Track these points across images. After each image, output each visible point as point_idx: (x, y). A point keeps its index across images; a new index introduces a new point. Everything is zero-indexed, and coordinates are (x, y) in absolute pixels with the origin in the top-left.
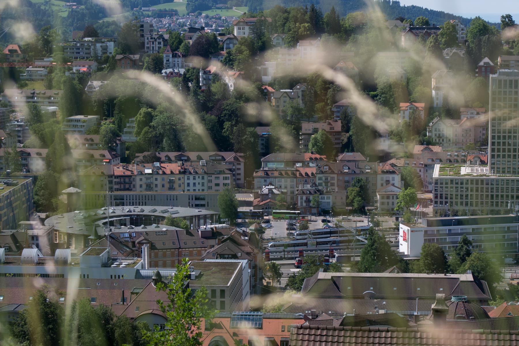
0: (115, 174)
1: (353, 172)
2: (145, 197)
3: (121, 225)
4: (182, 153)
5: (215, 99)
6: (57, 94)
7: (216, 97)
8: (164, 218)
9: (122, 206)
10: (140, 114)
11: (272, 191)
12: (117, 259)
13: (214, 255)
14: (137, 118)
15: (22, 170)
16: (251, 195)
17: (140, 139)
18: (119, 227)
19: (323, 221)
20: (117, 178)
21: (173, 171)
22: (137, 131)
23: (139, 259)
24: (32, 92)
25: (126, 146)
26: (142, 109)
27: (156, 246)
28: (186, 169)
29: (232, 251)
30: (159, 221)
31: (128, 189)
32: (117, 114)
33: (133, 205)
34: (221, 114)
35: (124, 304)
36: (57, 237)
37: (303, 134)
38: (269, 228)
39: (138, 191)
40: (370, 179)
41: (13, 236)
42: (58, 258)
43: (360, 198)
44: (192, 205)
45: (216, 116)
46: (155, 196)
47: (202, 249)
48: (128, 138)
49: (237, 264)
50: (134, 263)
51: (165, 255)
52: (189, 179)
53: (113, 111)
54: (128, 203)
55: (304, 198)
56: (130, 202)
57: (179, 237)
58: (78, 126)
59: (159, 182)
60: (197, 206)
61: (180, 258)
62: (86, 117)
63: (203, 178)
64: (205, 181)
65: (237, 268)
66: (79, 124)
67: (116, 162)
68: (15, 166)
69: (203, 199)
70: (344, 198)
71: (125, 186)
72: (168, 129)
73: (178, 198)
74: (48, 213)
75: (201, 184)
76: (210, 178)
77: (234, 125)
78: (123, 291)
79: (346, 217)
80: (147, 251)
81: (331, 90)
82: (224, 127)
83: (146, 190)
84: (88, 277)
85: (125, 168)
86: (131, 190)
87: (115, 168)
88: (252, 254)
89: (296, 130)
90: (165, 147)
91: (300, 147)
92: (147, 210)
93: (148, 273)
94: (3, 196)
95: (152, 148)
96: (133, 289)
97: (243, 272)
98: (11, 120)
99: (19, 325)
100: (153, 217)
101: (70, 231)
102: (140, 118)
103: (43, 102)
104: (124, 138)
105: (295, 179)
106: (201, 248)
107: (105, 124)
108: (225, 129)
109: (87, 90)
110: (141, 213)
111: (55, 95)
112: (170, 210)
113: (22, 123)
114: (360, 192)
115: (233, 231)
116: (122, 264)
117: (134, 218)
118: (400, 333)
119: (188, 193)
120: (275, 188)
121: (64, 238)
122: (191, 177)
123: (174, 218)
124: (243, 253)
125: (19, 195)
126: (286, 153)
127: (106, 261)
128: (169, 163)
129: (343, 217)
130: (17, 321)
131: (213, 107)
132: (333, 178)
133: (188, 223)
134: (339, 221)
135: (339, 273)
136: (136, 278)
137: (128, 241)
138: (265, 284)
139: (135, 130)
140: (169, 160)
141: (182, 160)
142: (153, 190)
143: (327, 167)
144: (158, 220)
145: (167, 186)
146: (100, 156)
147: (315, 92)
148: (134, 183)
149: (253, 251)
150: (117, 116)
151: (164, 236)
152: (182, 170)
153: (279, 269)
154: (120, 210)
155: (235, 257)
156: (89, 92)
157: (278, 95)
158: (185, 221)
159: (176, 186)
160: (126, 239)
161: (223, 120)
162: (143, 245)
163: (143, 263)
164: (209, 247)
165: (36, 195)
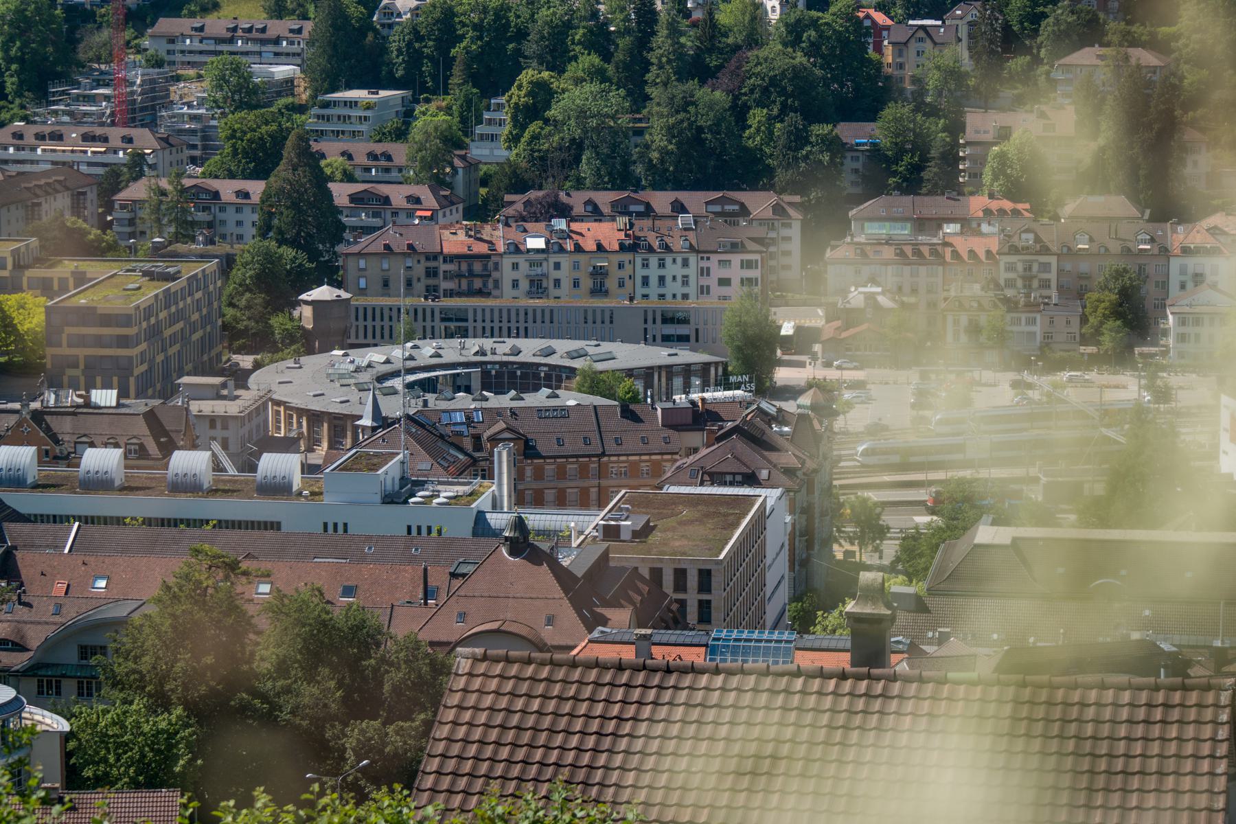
0: (446, 251)
1: (1102, 250)
2: (526, 314)
3: (458, 389)
4: (632, 195)
5: (728, 45)
6: (299, 31)
7: (730, 40)
8: (572, 371)
9: (462, 337)
10: (520, 87)
11: (876, 300)
12: (426, 482)
13: (693, 475)
14: (511, 97)
15: (194, 237)
16: (820, 312)
17: (517, 154)
18: (448, 393)
19: (1015, 385)
20: (451, 261)
21: (602, 242)
22: (511, 133)
23: (486, 482)
24: (231, 26)
25: (482, 173)
26: (524, 72)
27: (538, 448)
28: (638, 238)
29: (744, 464)
30: (559, 380)
31: (481, 293)
32: (459, 85)
33: (492, 336)
34: (740, 88)
35: (426, 604)
36: (280, 422)
37: (968, 144)
38: (863, 403)
39: (509, 298)
40: (1150, 270)
41: (151, 417)
42: (275, 477)
43: (1118, 323)
44: (654, 336)
45: (729, 92)
46: (552, 311)
47: (666, 457)
48: (486, 152)
49: (748, 501)
50: (471, 494)
51: (561, 474)
52: (647, 265)
53: (447, 78)
54: (480, 331)
55: (964, 320)
56: (484, 328)
57: (602, 424)
58: (353, 120)
59: (565, 274)
60: (667, 339)
61: (604, 483)
62: (373, 93)
63: (685, 263)
64: (692, 271)
65: (750, 511)
66: (355, 113)
67: (450, 218)
68: (177, 228)
69: (685, 321)
70: (1076, 321)
71: (470, 284)
72: (593, 129)
73: (614, 316)
74: (259, 357)
75: (679, 279)
76: (704, 264)
77: (777, 117)
78: (425, 570)
79: (1078, 373)
80: (508, 461)
81: (1051, 20)
82: (749, 122)
83: (530, 294)
84: (346, 531)
85: (472, 233)
86: (488, 295)
87: (446, 233)
88: (799, 474)
89: (949, 132)
90: (585, 178)
91: (961, 180)
92: (529, 349)
93: (536, 523)
94: (137, 308)
95: (551, 179)
96: (456, 563)
97: (769, 523)
98: (172, 101)
99: (128, 655)
100: (545, 369)
101: (316, 406)
102: (519, 96)
103: (260, 53)
104: (478, 151)
105: (940, 268)
106: (640, 455)
107: (424, 114)
108: (752, 130)
109: (378, 19)
110: (512, 359)
111: (291, 35)
112: (591, 350)
113: (200, 111)
114: (1121, 305)
115: (749, 410)
116: (438, 496)
117: (493, 372)
118: (748, 677)
119: (644, 304)
120: (883, 293)
121: (300, 425)
122: (653, 261)
123: (601, 372)
124: (774, 472)
125: (181, 305)
126: (920, 194)
127: (397, 487)
128: (596, 221)
129: (1073, 373)
130: (124, 644)
131: (720, 68)
132: (1045, 267)
133: (639, 386)
134: (1056, 386)
135: (1102, 531)
136: (475, 534)
137: (460, 434)
138: (839, 556)
139: (506, 130)
140: (596, 213)
141: (629, 214)
142: (548, 297)
143: (1031, 236)
144: (557, 377)
145: (587, 283)
146: (237, 197)
147: (1007, 27)
148: (495, 275)
149: (803, 463)
150: (457, 91)
151: (561, 420)
152: (628, 242)
153: (879, 515)
154: (453, 350)
155: (751, 479)
156: (383, 25)
157: (901, 35)
158: (628, 382)
159: (611, 284)
160: (458, 428)
161: (745, 104)
162: (496, 446)
163: (496, 493)
164: (683, 452)
165: (231, 305)
